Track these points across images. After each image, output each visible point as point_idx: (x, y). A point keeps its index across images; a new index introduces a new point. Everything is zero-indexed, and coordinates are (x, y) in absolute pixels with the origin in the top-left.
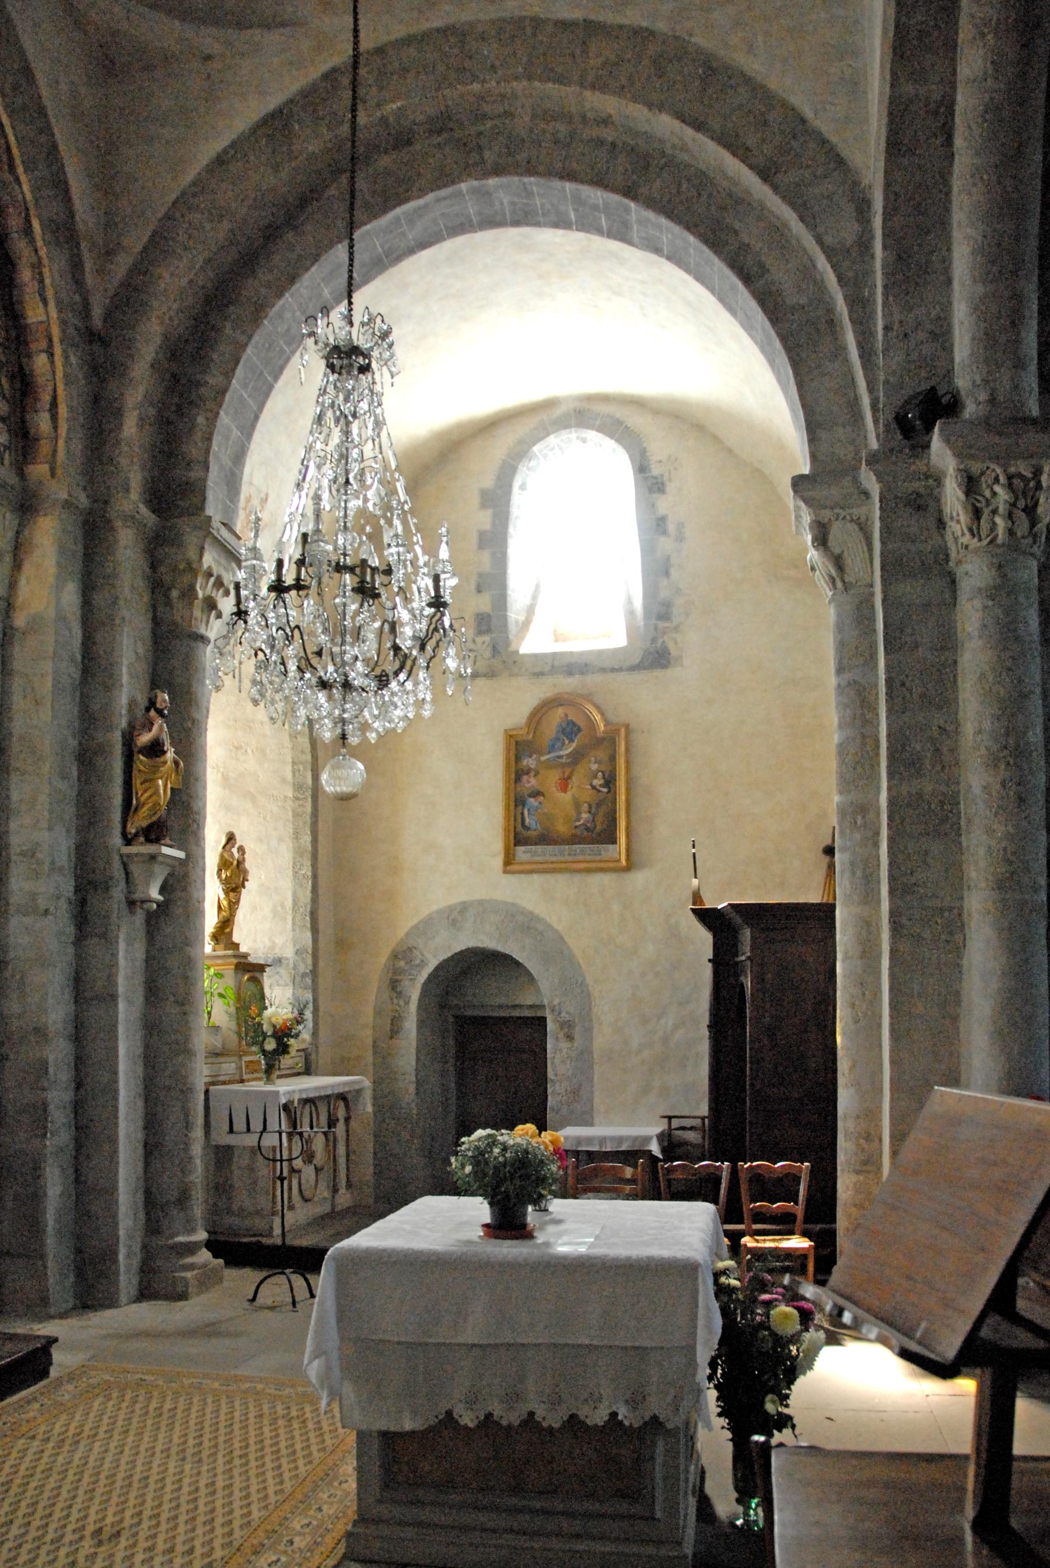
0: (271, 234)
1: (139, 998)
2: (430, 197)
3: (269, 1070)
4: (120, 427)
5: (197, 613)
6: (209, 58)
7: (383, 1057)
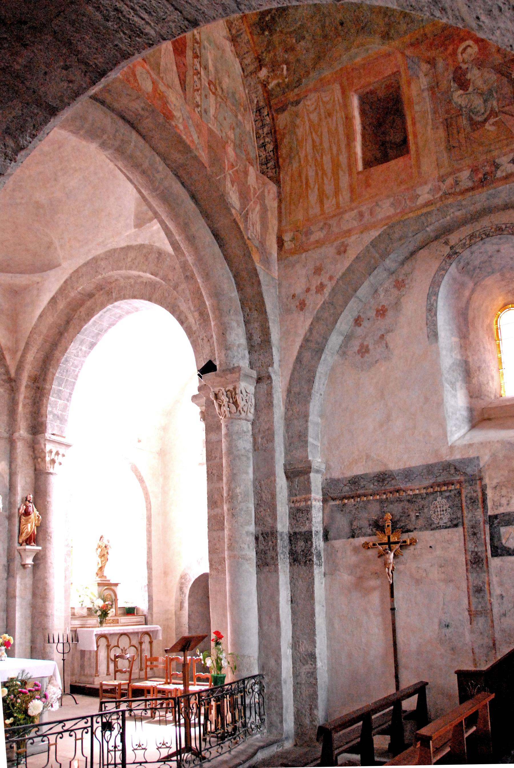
0: (61, 334)
1: (29, 596)
2: (101, 313)
3: (101, 623)
4: (18, 409)
5: (48, 465)
6: (38, 283)
7: (178, 617)
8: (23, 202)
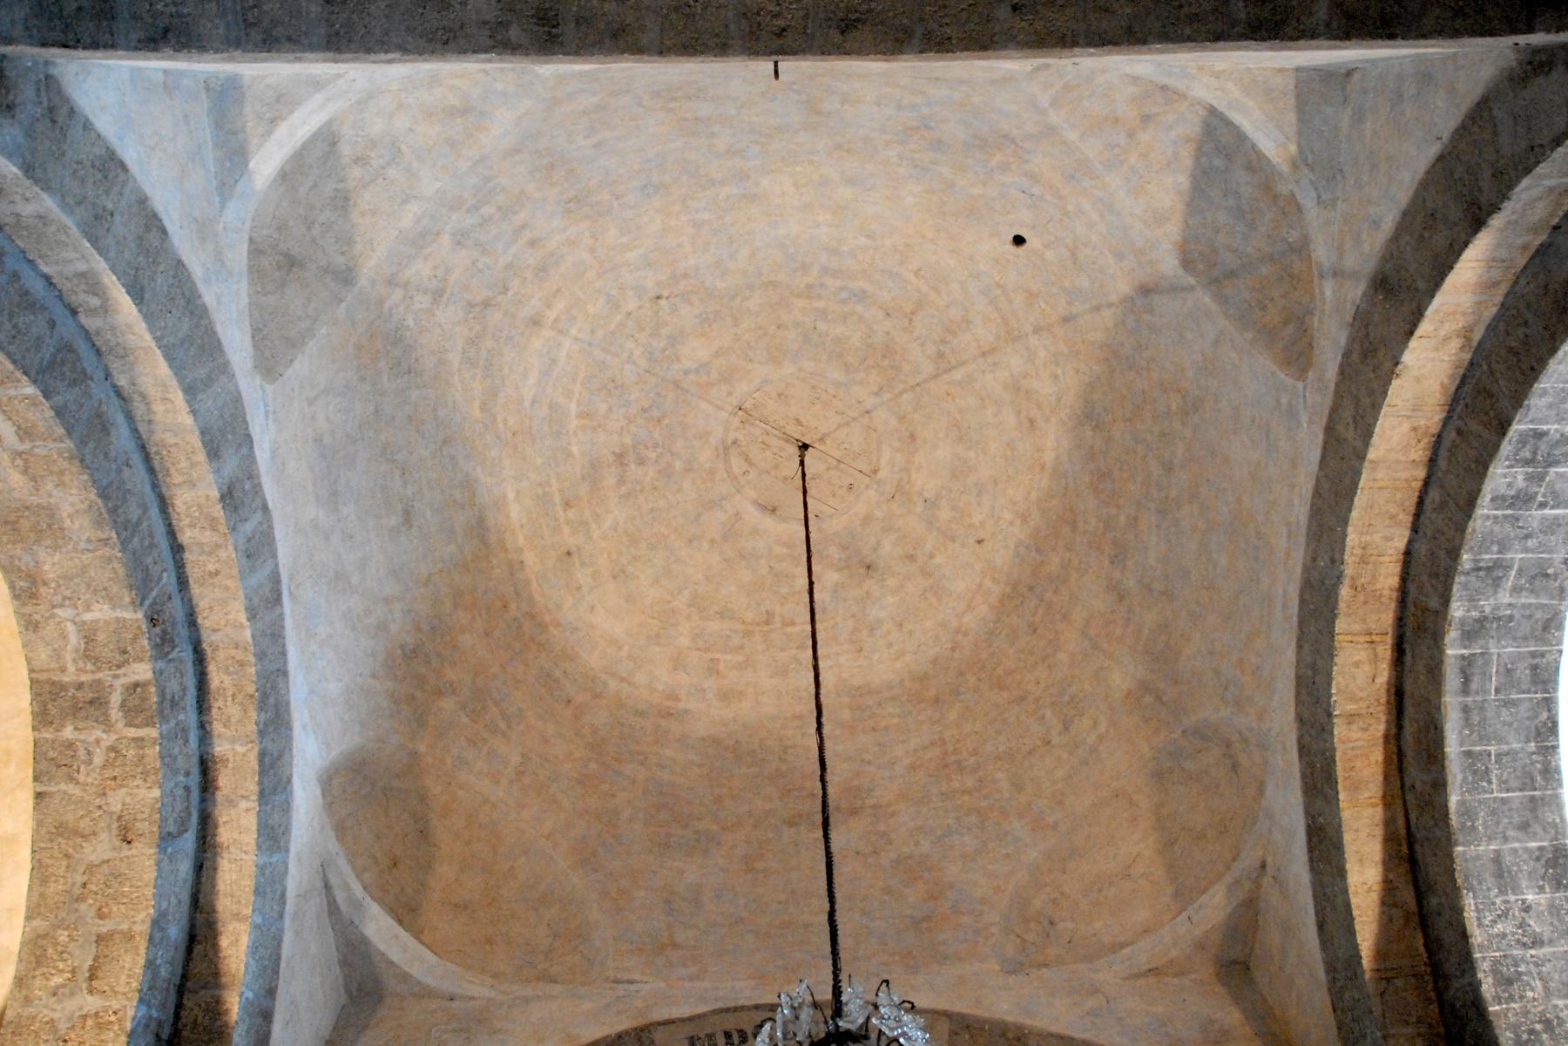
8: (1102, 729)
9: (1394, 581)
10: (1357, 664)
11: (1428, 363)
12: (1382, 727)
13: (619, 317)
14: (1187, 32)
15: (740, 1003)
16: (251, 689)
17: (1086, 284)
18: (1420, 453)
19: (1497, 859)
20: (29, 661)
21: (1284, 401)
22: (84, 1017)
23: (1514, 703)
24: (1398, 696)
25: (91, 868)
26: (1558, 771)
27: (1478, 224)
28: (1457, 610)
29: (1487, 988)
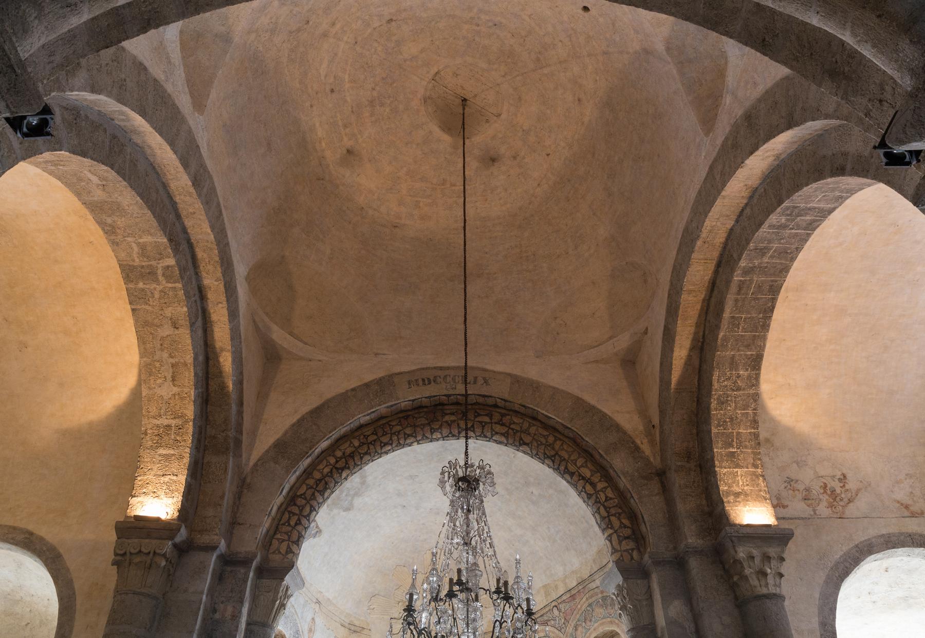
9: (723, 240)
10: (698, 271)
11: (757, 164)
12: (703, 296)
13: (369, 31)
14: (673, 10)
15: (429, 365)
16: (217, 259)
17: (618, 39)
18: (746, 194)
19: (733, 357)
20: (116, 257)
21: (697, 140)
22: (174, 395)
23: (758, 299)
24: (713, 285)
25: (162, 338)
26: (769, 326)
27: (789, 127)
28: (743, 263)
29: (714, 404)
